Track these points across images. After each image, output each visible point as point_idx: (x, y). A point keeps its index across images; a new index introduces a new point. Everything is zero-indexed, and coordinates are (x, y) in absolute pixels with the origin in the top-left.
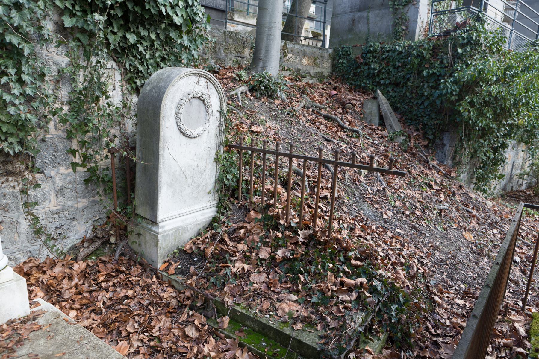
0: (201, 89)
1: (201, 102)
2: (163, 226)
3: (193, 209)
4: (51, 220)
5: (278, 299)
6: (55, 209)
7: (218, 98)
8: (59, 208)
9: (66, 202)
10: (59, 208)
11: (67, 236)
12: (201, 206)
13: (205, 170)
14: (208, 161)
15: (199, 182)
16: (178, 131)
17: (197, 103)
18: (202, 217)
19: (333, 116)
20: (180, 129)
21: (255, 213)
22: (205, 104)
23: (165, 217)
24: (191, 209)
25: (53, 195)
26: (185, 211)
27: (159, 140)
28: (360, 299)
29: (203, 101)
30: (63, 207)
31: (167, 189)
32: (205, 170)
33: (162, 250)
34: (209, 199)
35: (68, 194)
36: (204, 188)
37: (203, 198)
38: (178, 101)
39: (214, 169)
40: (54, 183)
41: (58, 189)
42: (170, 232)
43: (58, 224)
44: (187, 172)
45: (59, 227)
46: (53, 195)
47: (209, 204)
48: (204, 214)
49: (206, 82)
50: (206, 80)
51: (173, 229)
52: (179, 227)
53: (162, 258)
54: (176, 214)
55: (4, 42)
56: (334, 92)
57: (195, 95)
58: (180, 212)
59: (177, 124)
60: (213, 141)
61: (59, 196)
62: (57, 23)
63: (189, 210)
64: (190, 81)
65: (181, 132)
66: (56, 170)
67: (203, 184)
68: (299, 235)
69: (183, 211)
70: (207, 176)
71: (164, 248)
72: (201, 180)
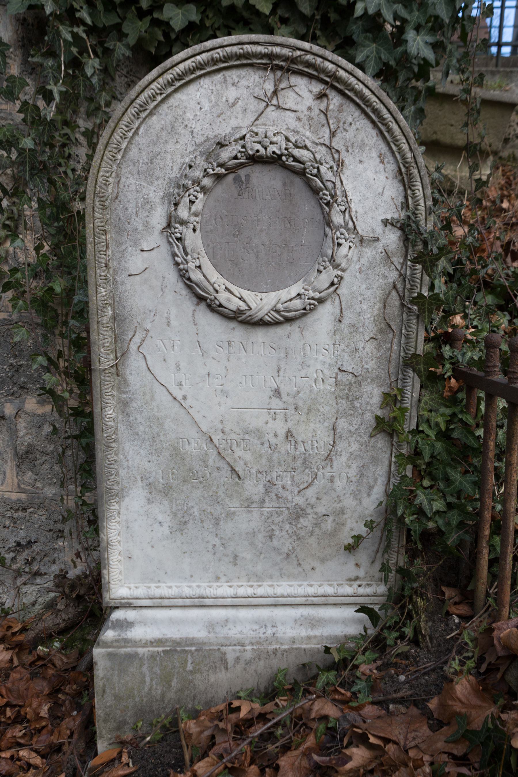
0: (293, 124)
2: (127, 624)
3: (270, 591)
4: (7, 523)
6: (14, 496)
7: (391, 167)
8: (23, 496)
9: (39, 485)
10: (23, 496)
11: (43, 570)
12: (311, 591)
13: (328, 458)
14: (342, 424)
15: (300, 501)
18: (304, 632)
21: (475, 691)
22: (315, 191)
24: (260, 591)
25: (9, 463)
26: (230, 592)
30: (33, 498)
31: (150, 501)
32: (328, 458)
33: (109, 700)
34: (350, 570)
35: (46, 466)
36: (329, 525)
37: (323, 560)
38: (175, 173)
39: (375, 460)
40: (13, 433)
41: (22, 450)
42: (141, 651)
43: (22, 535)
44: (239, 452)
45: (24, 543)
46: (9, 463)
47: (349, 590)
48: (314, 623)
49: (321, 96)
50: (317, 88)
51: (159, 642)
52: (191, 642)
53: (111, 725)
58: (209, 592)
59: (177, 264)
60: (370, 347)
61: (24, 467)
62: (25, 19)
63: (250, 591)
64: (232, 93)
65: (201, 299)
66: (17, 401)
67: (321, 510)
70: (339, 484)
71: (117, 698)
72: (310, 493)
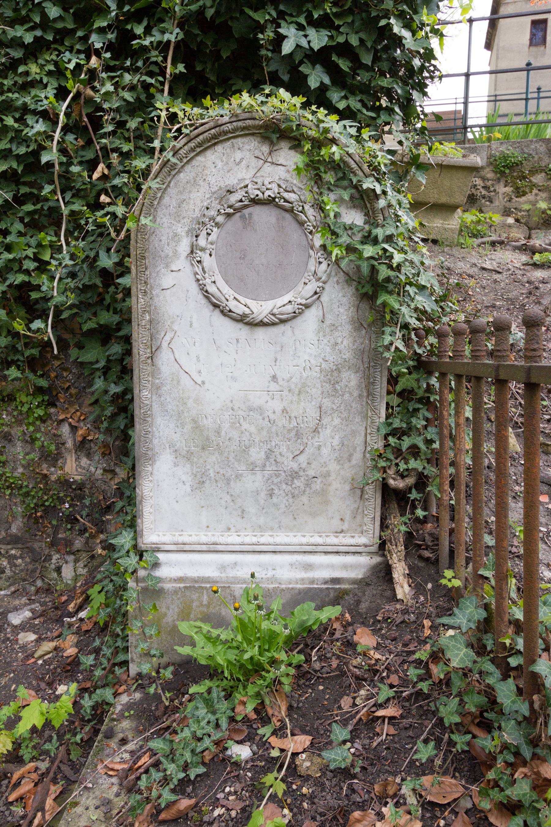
1: (287, 216)
3: (271, 540)
5: (83, 374)
16: (204, 301)
17: (273, 220)
20: (206, 295)
24: (263, 540)
26: (239, 540)
27: (131, 312)
29: (291, 211)
31: (176, 465)
32: (316, 431)
51: (180, 580)
54: (204, 539)
56: (258, 635)
57: (254, 193)
58: (221, 540)
63: (254, 540)
67: (311, 473)
68: (319, 608)
69: (233, 539)
70: (325, 451)
72: (302, 459)
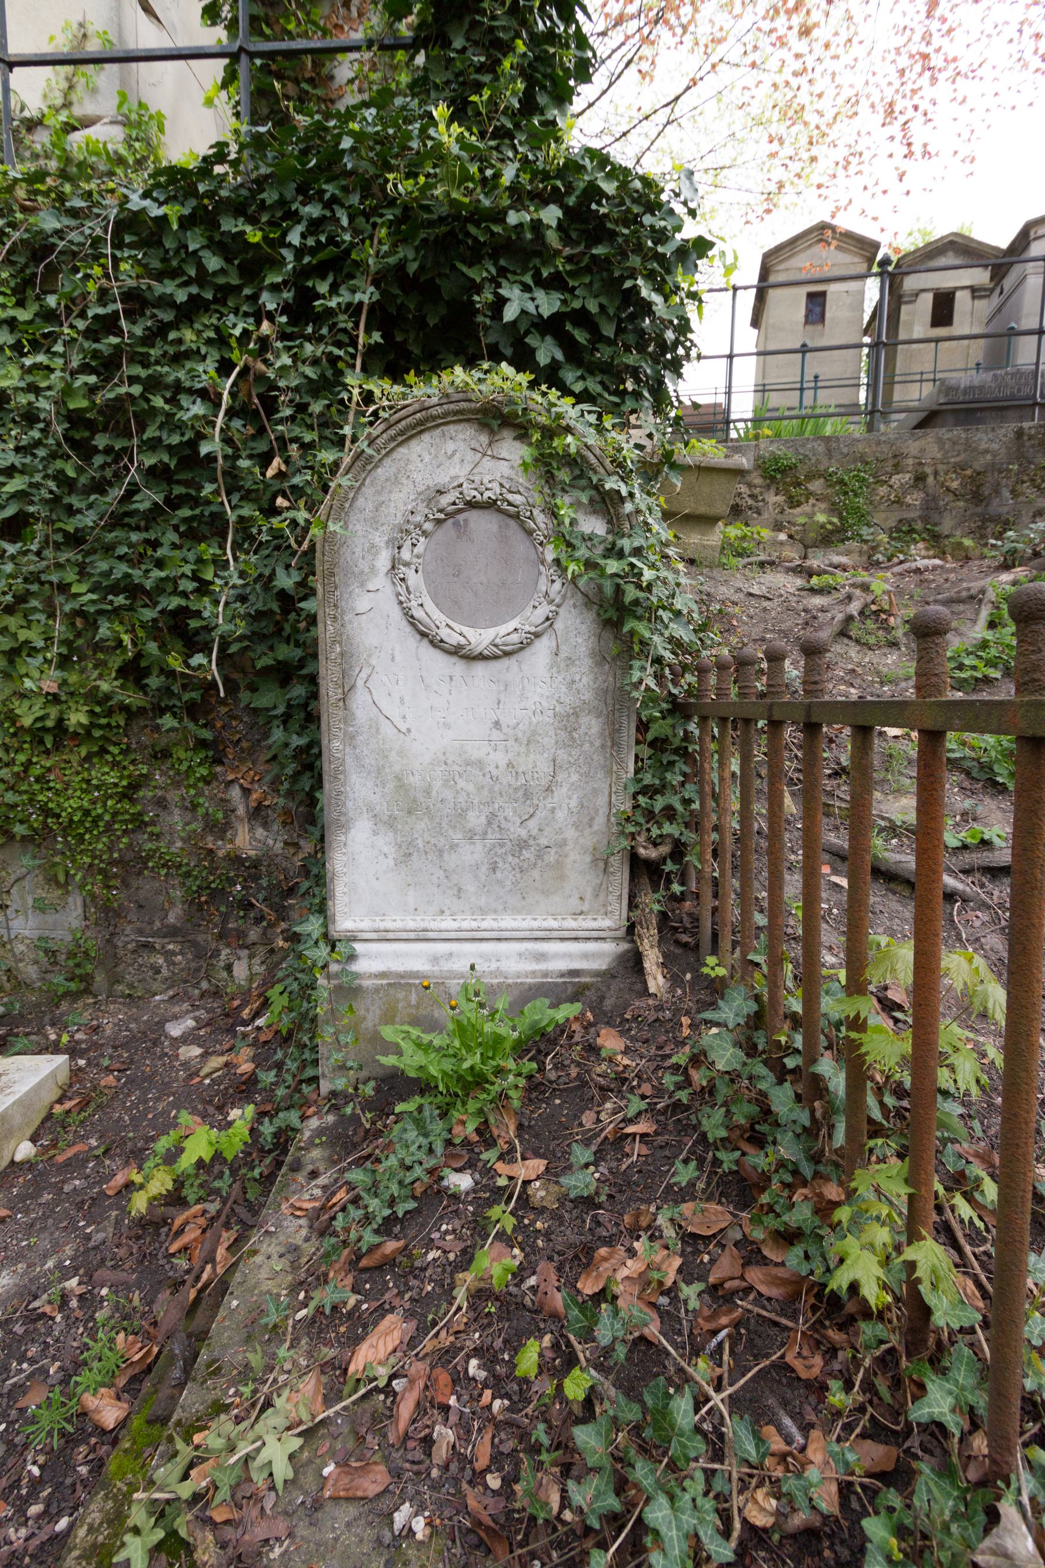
12: (535, 924)
16: (408, 629)
17: (494, 527)
19: (369, 1150)
20: (412, 621)
23: (365, 925)
24: (484, 925)
26: (455, 925)
28: (749, 1140)
29: (516, 517)
31: (375, 833)
32: (549, 789)
51: (383, 975)
52: (415, 975)
54: (411, 925)
55: (755, 1192)
58: (433, 925)
63: (474, 925)
64: (450, 446)
69: (447, 923)
72: (532, 824)
